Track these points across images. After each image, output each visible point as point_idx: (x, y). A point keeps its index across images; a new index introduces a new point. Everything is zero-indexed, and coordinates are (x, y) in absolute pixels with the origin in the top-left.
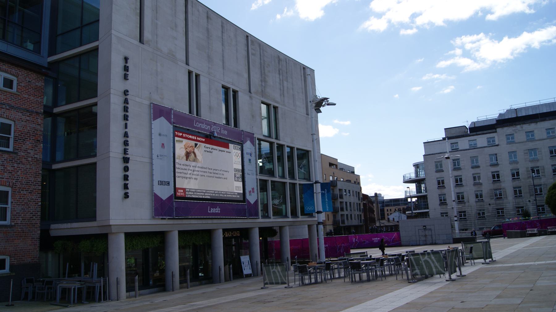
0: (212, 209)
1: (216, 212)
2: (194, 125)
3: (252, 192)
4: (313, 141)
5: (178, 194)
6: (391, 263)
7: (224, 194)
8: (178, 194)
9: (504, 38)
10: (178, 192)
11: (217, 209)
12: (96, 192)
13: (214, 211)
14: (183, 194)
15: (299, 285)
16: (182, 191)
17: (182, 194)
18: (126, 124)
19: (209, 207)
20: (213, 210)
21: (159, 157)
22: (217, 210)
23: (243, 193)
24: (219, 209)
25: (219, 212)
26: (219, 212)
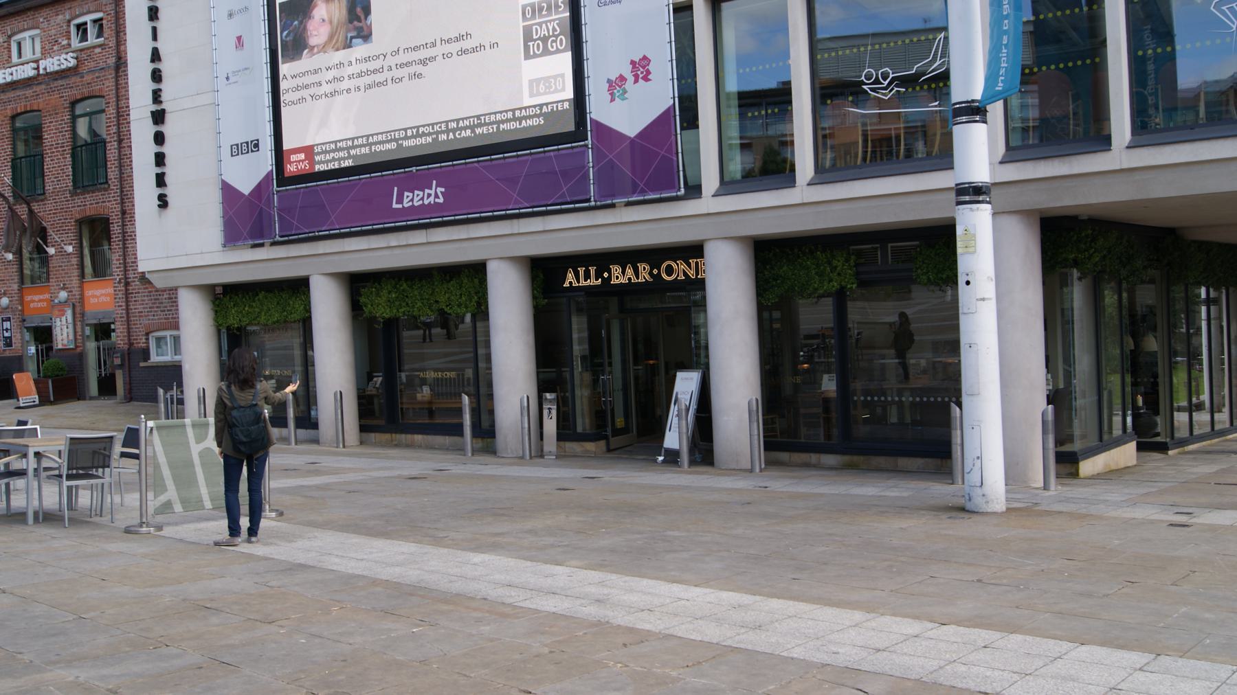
0: (406, 194)
1: (426, 202)
2: (1212, 8)
3: (631, 78)
4: (714, 657)
5: (291, 169)
6: (1074, 12)
7: (472, 128)
8: (291, 169)
9: (268, 449)
10: (290, 163)
11: (432, 192)
12: (698, 120)
13: (416, 199)
14: (304, 167)
15: (1208, 429)
16: (302, 156)
17: (301, 166)
18: (154, 30)
19: (396, 188)
20: (414, 199)
21: (232, 79)
22: (433, 195)
23: (574, 98)
24: (440, 190)
25: (441, 200)
26: (441, 200)
